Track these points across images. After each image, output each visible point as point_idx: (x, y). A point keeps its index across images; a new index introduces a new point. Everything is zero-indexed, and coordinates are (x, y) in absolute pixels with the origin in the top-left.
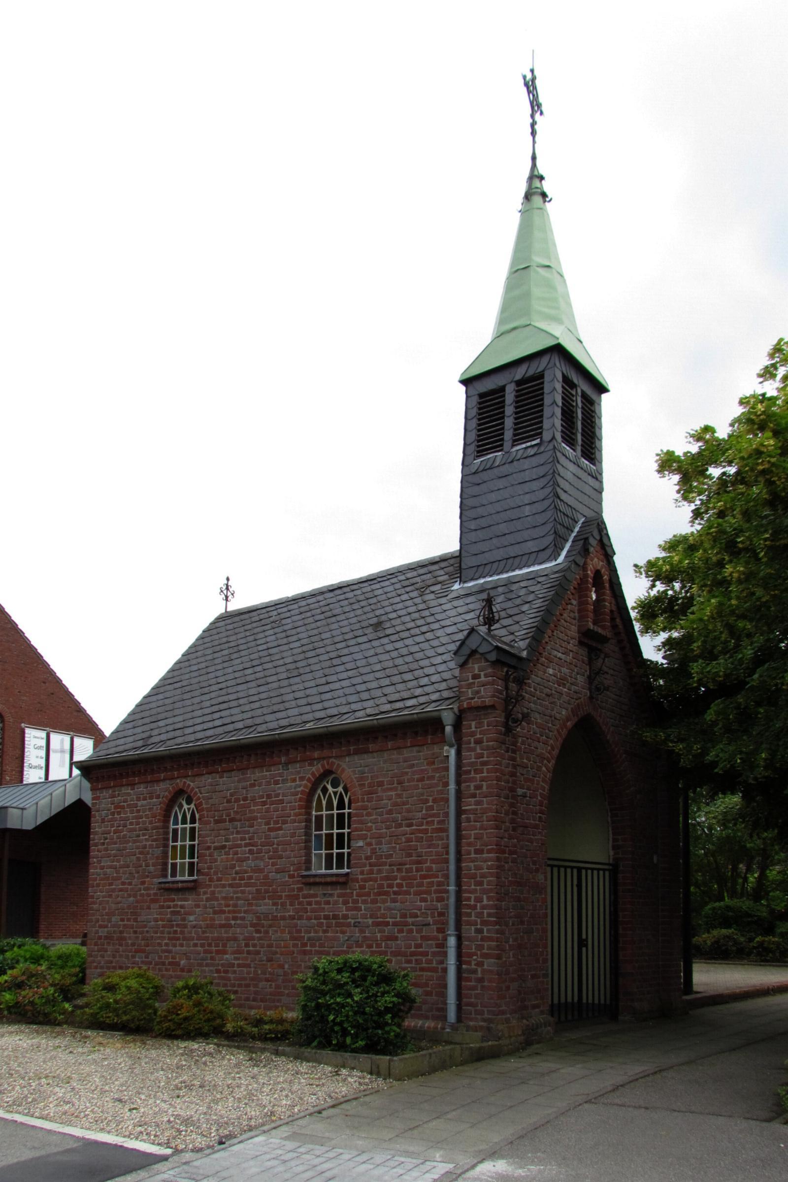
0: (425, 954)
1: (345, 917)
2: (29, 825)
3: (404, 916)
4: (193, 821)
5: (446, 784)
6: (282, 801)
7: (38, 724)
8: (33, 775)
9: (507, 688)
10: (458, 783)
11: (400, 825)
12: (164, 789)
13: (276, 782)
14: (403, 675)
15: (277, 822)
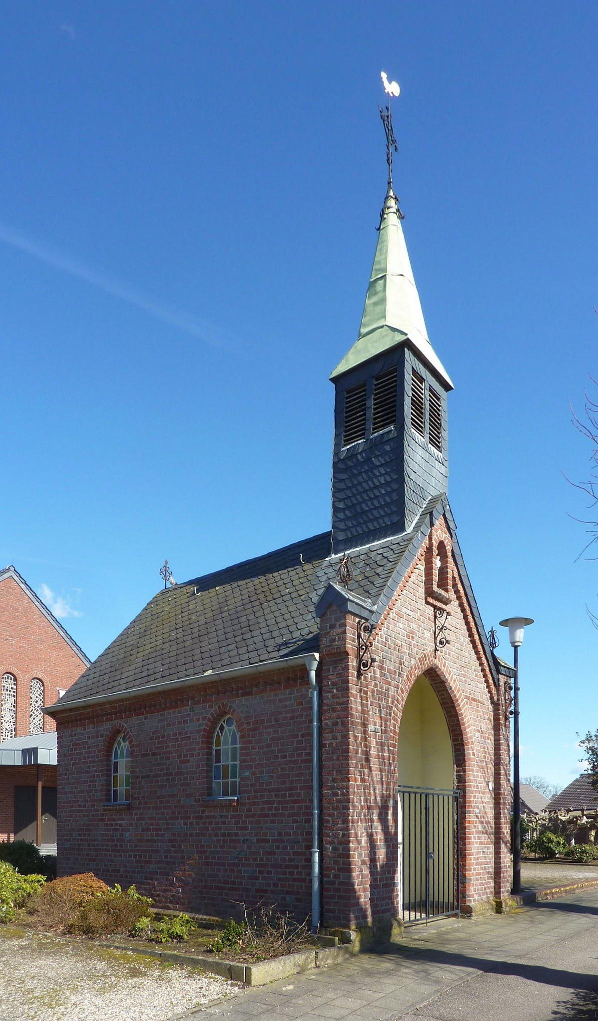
0: (297, 867)
1: (237, 835)
3: (280, 834)
5: (311, 721)
9: (359, 636)
10: (320, 721)
11: (277, 757)
12: (106, 727)
13: (186, 722)
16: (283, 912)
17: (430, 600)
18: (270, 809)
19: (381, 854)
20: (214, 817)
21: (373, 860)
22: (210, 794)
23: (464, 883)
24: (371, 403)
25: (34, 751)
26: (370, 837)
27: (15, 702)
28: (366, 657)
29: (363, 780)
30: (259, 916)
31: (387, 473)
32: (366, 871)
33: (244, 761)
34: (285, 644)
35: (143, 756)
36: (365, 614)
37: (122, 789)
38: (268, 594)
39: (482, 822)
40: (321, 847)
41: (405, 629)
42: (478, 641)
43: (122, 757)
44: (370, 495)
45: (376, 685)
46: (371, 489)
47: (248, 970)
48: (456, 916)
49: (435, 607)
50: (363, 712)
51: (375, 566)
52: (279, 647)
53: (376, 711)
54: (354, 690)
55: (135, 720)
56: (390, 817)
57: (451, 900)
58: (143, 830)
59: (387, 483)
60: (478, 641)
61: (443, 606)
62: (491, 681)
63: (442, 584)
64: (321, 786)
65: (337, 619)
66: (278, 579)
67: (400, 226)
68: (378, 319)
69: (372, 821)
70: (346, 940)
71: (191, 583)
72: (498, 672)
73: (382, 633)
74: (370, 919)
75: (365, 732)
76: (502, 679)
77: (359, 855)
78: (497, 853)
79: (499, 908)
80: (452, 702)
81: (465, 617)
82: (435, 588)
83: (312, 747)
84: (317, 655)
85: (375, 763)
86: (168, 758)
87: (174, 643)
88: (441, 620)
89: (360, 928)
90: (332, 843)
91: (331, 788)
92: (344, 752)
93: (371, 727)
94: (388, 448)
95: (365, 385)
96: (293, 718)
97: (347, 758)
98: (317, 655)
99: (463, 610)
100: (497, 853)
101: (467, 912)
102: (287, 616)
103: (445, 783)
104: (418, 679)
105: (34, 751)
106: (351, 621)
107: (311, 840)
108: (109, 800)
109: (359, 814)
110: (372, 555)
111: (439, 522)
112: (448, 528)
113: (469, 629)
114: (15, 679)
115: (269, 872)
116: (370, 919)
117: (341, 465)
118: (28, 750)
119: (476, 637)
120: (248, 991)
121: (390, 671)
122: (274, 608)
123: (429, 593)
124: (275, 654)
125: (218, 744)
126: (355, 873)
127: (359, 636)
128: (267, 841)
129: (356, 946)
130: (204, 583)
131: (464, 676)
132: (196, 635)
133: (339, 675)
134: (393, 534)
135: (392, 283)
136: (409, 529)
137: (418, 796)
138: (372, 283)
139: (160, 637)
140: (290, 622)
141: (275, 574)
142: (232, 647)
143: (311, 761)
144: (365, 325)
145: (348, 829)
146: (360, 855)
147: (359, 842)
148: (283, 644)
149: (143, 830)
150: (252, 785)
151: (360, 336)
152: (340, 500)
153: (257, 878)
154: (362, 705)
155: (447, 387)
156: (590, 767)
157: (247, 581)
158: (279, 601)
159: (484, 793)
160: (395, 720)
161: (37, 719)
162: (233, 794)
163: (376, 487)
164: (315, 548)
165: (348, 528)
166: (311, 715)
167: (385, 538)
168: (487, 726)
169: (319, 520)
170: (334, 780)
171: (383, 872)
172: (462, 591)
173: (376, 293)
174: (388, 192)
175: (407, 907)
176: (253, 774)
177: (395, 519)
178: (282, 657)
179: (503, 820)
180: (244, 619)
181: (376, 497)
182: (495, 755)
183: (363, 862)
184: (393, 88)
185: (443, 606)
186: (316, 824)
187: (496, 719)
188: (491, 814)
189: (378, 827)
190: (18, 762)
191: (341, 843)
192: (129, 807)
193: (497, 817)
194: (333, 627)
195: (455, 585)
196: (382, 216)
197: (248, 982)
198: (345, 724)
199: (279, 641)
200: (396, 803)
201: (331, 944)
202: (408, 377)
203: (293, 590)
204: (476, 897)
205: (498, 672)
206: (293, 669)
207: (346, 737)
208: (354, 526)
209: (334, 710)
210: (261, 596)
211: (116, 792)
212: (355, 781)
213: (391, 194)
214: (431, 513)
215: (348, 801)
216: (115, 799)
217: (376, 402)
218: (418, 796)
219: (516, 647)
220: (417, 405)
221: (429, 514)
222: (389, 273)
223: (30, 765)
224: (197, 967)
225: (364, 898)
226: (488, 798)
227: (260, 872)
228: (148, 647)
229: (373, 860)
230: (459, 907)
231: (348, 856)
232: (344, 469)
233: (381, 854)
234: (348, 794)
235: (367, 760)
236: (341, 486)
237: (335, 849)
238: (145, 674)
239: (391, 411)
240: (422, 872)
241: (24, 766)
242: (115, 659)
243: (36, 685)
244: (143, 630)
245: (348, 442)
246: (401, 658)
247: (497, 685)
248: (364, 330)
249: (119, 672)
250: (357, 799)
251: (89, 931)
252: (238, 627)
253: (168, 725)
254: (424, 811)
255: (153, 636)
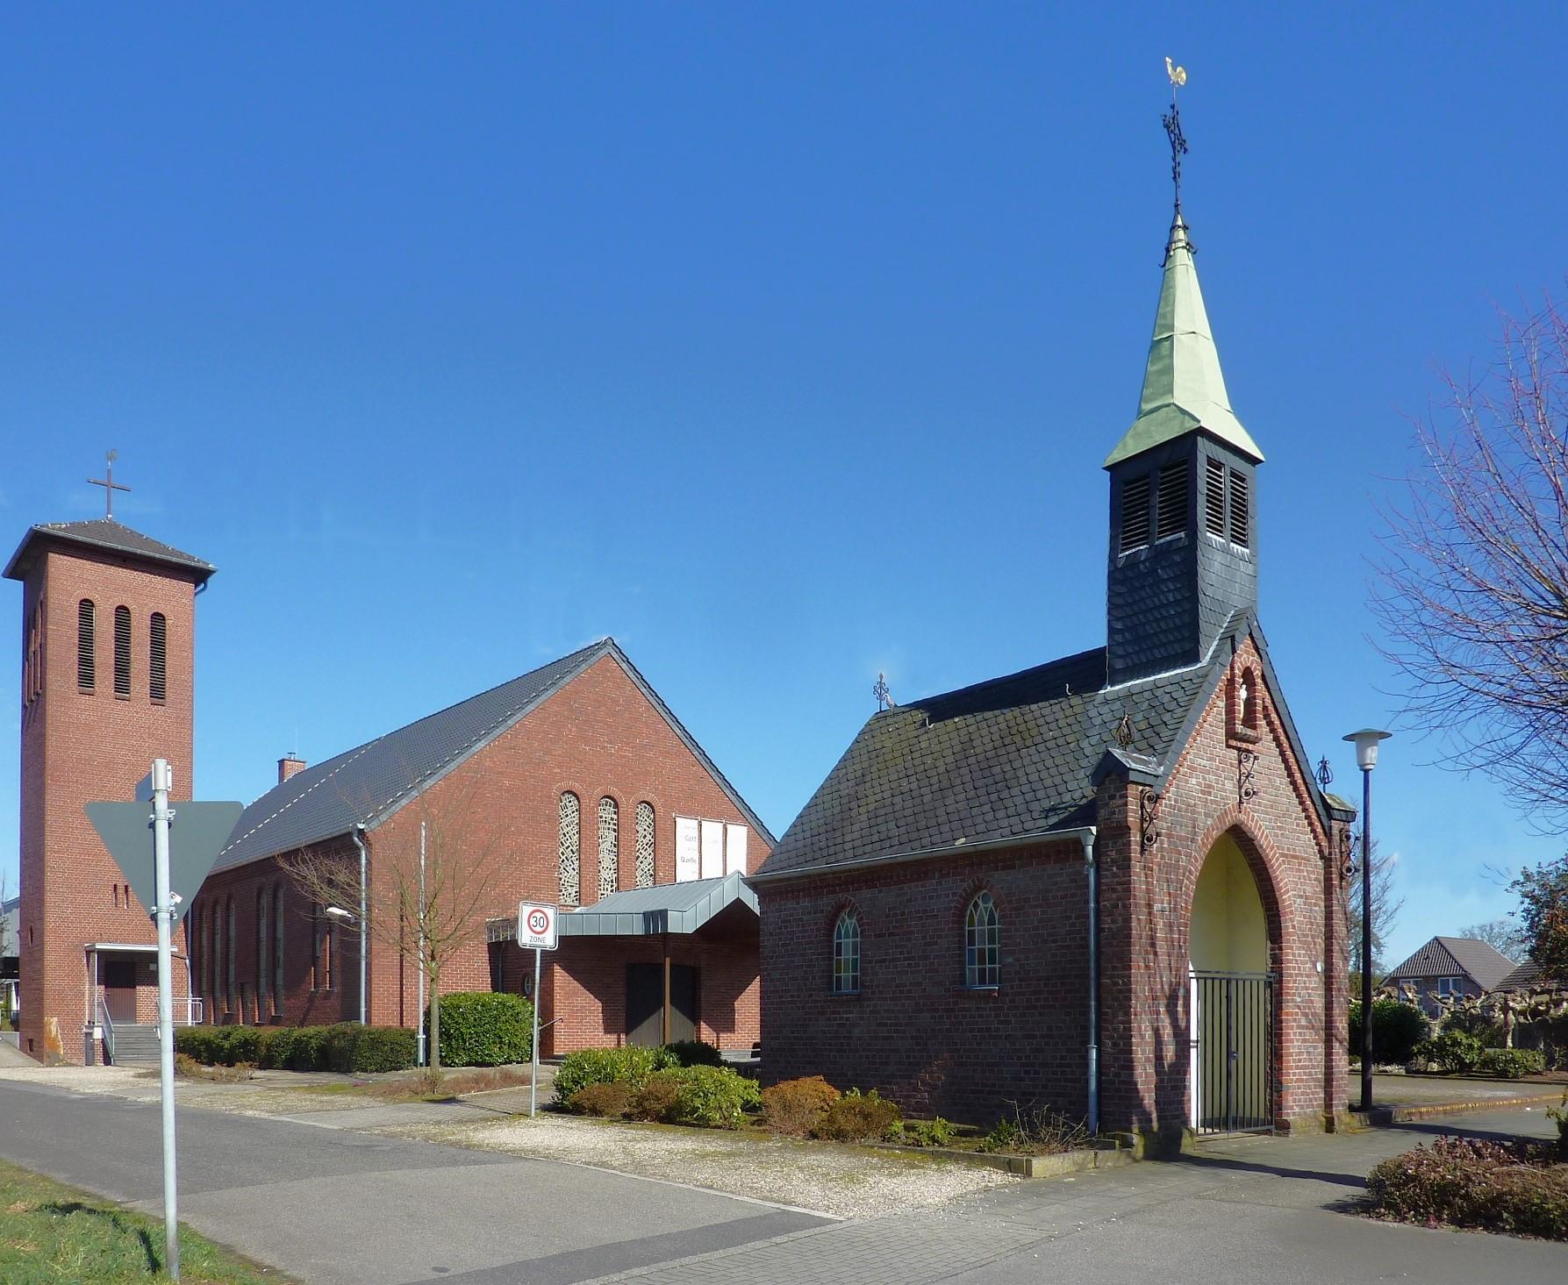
0: (1070, 1066)
1: (997, 1030)
2: (690, 930)
3: (1050, 1028)
4: (855, 935)
5: (1087, 902)
6: (936, 916)
7: (688, 813)
8: (686, 872)
9: (1142, 806)
10: (1097, 902)
11: (1045, 942)
12: (827, 902)
13: (931, 898)
14: (1360, 876)
15: (932, 937)
16: (1058, 1112)
17: (1234, 743)
18: (1038, 1000)
19: (1170, 1053)
20: (969, 1010)
21: (1159, 1058)
22: (963, 982)
23: (1279, 1091)
24: (1156, 499)
25: (662, 915)
26: (1157, 1033)
27: (617, 838)
28: (1151, 831)
29: (1147, 967)
30: (1029, 1116)
31: (1177, 589)
32: (1151, 1070)
33: (1005, 945)
34: (1053, 809)
35: (877, 936)
36: (1149, 780)
37: (847, 975)
38: (1026, 735)
39: (1306, 1015)
40: (1099, 1043)
41: (1202, 780)
42: (1300, 781)
43: (847, 936)
44: (1157, 610)
45: (1163, 857)
46: (1157, 608)
47: (1029, 1161)
48: (1268, 1132)
49: (1239, 749)
50: (1148, 891)
51: (1161, 711)
52: (1047, 813)
53: (1164, 886)
54: (1136, 867)
55: (866, 893)
56: (1180, 1009)
57: (1262, 1116)
58: (879, 1025)
59: (1177, 602)
60: (1300, 781)
61: (1251, 747)
62: (1319, 830)
63: (1249, 721)
64: (1099, 974)
65: (1117, 789)
66: (1037, 714)
67: (1191, 263)
68: (1163, 394)
69: (1158, 1013)
70: (1127, 1144)
71: (917, 706)
72: (1330, 818)
73: (1170, 796)
74: (1155, 1125)
75: (1150, 913)
76: (1336, 826)
77: (1142, 1053)
78: (1329, 1054)
79: (1330, 1126)
80: (1263, 863)
81: (1282, 754)
82: (1239, 728)
83: (1088, 931)
84: (1094, 829)
85: (1162, 948)
86: (909, 940)
87: (907, 796)
88: (1248, 765)
89: (1145, 1132)
90: (1111, 1038)
91: (1111, 977)
92: (1124, 936)
93: (1157, 907)
94: (1177, 558)
95: (1146, 477)
96: (1064, 897)
97: (1129, 944)
98: (1094, 829)
99: (1279, 745)
100: (1329, 1054)
101: (1284, 1127)
102: (1053, 771)
103: (1256, 964)
104: (1218, 841)
105: (662, 915)
106: (1133, 791)
107: (1088, 1036)
108: (831, 989)
109: (1143, 1006)
110: (1159, 692)
111: (1244, 646)
112: (1257, 649)
113: (1288, 768)
114: (616, 806)
115: (1036, 1073)
116: (1155, 1125)
117: (1118, 576)
118: (652, 913)
119: (1298, 775)
120: (1029, 1181)
121: (1180, 838)
122: (1036, 758)
123: (1231, 734)
124: (1042, 823)
125: (971, 923)
126: (1139, 1071)
127: (1142, 806)
128: (1034, 1037)
129: (1139, 1151)
130: (940, 708)
131: (1280, 828)
132: (935, 787)
133: (1119, 852)
134: (1185, 665)
135: (1182, 344)
136: (1205, 661)
137: (1217, 982)
138: (1159, 347)
139: (886, 787)
140: (1058, 780)
141: (1033, 707)
142: (987, 808)
143: (1088, 946)
144: (1150, 400)
145: (1130, 1022)
146: (1144, 1052)
147: (1142, 1037)
148: (1050, 810)
149: (879, 1025)
150: (1017, 973)
151: (1141, 414)
152: (1118, 619)
153: (1022, 1080)
154: (1147, 883)
155: (1254, 461)
156: (1526, 925)
157: (997, 712)
158: (1041, 748)
159: (1308, 976)
160: (1187, 895)
161: (646, 862)
162: (992, 982)
163: (1163, 605)
164: (1081, 673)
165: (1128, 654)
166: (1087, 894)
167: (1175, 668)
168: (1314, 888)
169: (1087, 630)
170: (1114, 968)
171: (1171, 1072)
172: (1277, 722)
173: (1161, 358)
174: (1175, 219)
175: (1205, 1123)
176: (1018, 960)
177: (1188, 646)
178: (1052, 827)
179: (1336, 1011)
180: (997, 770)
181: (1163, 618)
182: (1326, 925)
183: (1148, 1060)
184: (1180, 76)
185: (1251, 747)
186: (1093, 1016)
187: (1328, 879)
188: (1319, 1004)
189: (1165, 1021)
190: (638, 930)
191: (1121, 1037)
192: (859, 998)
193: (1329, 1007)
194: (1112, 797)
195: (1267, 716)
196: (1168, 250)
197: (1029, 1174)
198: (1127, 907)
199: (1046, 804)
200: (1188, 991)
201: (1112, 1147)
202: (1202, 469)
203: (1057, 733)
204: (1297, 1110)
205: (1330, 818)
206: (1066, 842)
207: (1128, 920)
208: (1137, 653)
209: (1114, 890)
210: (1017, 739)
211: (839, 979)
212: (1138, 972)
213: (1180, 223)
214: (1233, 638)
215: (1130, 991)
216: (839, 988)
217: (1163, 495)
218: (1217, 982)
219: (1366, 772)
220: (1214, 500)
221: (1231, 639)
222: (1177, 332)
223: (656, 934)
224: (975, 1160)
225: (1149, 1100)
226: (1315, 984)
227: (1027, 1072)
228: (871, 799)
229: (1159, 1058)
230: (1275, 1122)
231: (1130, 1052)
232: (1122, 580)
233: (1170, 1053)
234: (1130, 983)
235: (1153, 945)
236: (1119, 601)
237: (1115, 1044)
238: (876, 838)
239: (1183, 516)
240: (1222, 1078)
241: (647, 936)
242: (829, 813)
243: (644, 811)
244: (859, 774)
245: (1127, 546)
246: (1195, 820)
247: (1328, 834)
248: (1146, 407)
249: (838, 833)
250: (1141, 987)
251: (840, 1136)
252: (991, 781)
253: (909, 901)
254: (1224, 1000)
255: (875, 783)
